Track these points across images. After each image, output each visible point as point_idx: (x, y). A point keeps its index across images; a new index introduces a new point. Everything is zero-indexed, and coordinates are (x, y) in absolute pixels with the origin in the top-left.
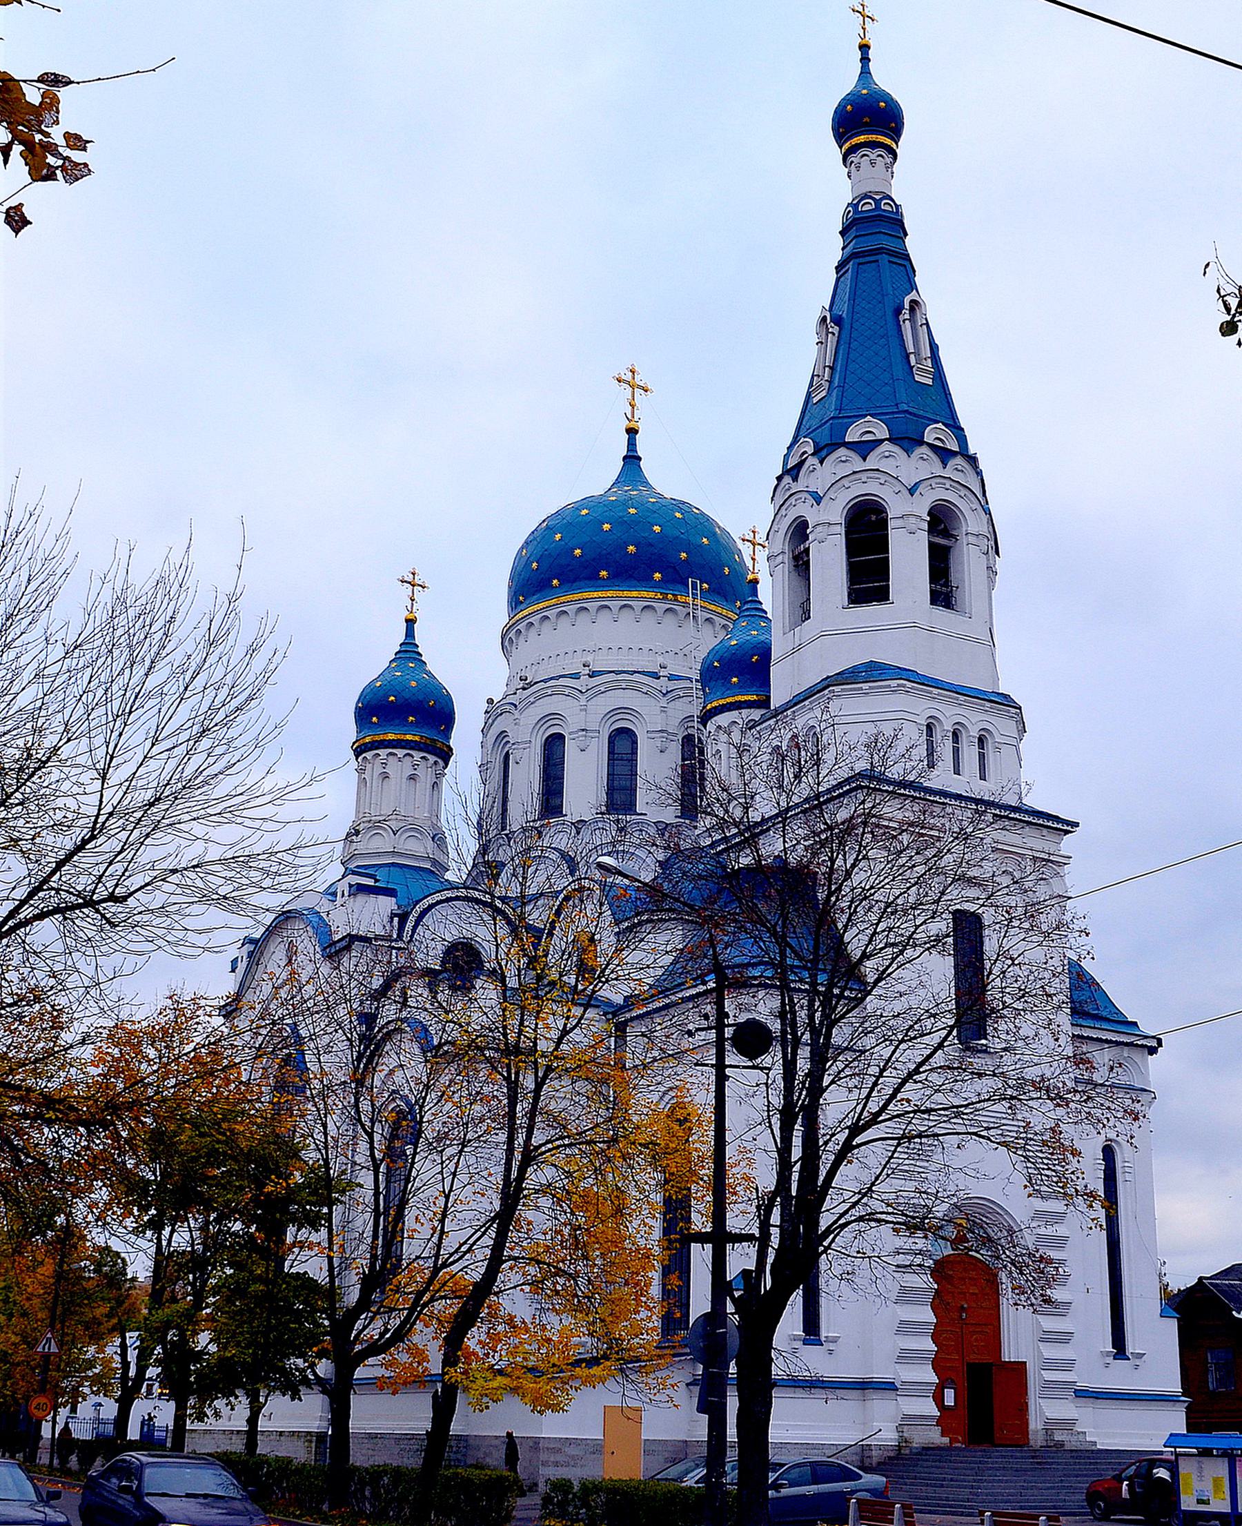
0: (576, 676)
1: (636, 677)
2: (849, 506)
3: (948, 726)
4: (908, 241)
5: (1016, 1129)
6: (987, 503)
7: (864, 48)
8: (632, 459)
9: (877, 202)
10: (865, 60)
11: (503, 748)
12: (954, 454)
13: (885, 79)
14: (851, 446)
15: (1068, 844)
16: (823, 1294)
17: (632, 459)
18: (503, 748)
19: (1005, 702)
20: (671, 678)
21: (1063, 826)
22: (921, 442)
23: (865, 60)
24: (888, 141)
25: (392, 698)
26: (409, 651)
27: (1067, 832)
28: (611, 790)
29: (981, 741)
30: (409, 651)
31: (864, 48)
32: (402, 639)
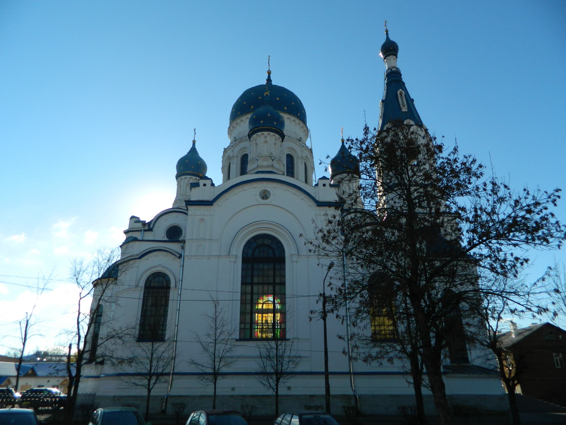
4: (402, 77)
7: (387, 31)
9: (391, 69)
10: (387, 34)
11: (242, 153)
18: (242, 153)
23: (387, 34)
24: (395, 53)
26: (193, 150)
30: (193, 150)
31: (387, 31)
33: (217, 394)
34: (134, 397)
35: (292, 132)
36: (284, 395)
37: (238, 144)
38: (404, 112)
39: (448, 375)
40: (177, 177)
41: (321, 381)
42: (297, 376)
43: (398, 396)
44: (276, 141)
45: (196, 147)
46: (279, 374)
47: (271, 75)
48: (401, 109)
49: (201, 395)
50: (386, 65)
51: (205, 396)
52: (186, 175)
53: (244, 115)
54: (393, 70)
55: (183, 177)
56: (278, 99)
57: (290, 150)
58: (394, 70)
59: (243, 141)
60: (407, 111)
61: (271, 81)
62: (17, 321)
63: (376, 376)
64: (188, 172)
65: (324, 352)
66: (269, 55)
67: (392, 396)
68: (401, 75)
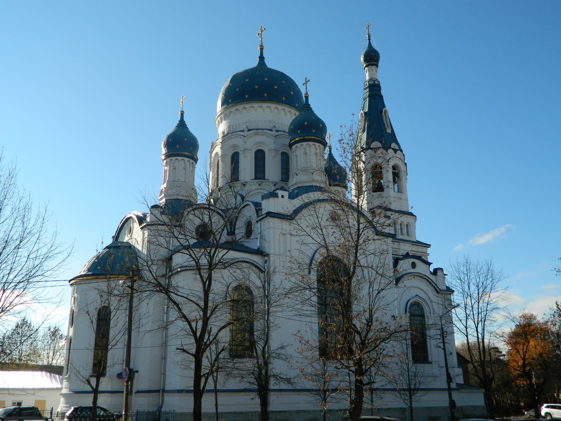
0: (243, 131)
1: (265, 131)
2: (419, 302)
3: (405, 223)
4: (382, 91)
5: (373, 305)
6: (404, 160)
8: (262, 58)
9: (374, 81)
11: (257, 147)
12: (398, 150)
13: (375, 46)
14: (393, 149)
15: (429, 250)
16: (428, 337)
17: (262, 58)
19: (411, 214)
20: (277, 131)
21: (428, 246)
22: (390, 148)
25: (186, 140)
26: (182, 124)
27: (428, 247)
28: (183, 115)
29: (407, 226)
30: (182, 124)
32: (179, 119)
33: (219, 411)
34: (235, 413)
35: (281, 124)
36: (303, 410)
37: (252, 135)
38: (389, 133)
39: (461, 391)
40: (168, 156)
41: (446, 395)
42: (431, 392)
43: (431, 408)
44: (305, 150)
45: (185, 119)
46: (411, 391)
47: (264, 51)
48: (385, 129)
49: (297, 411)
50: (367, 74)
51: (300, 411)
52: (183, 157)
53: (257, 103)
54: (376, 82)
55: (174, 158)
56: (276, 87)
57: (283, 148)
58: (371, 83)
59: (260, 134)
60: (390, 132)
61: (264, 58)
62: (91, 329)
63: (437, 392)
64: (313, 138)
65: (446, 376)
66: (265, 28)
67: (428, 408)
68: (310, 105)
